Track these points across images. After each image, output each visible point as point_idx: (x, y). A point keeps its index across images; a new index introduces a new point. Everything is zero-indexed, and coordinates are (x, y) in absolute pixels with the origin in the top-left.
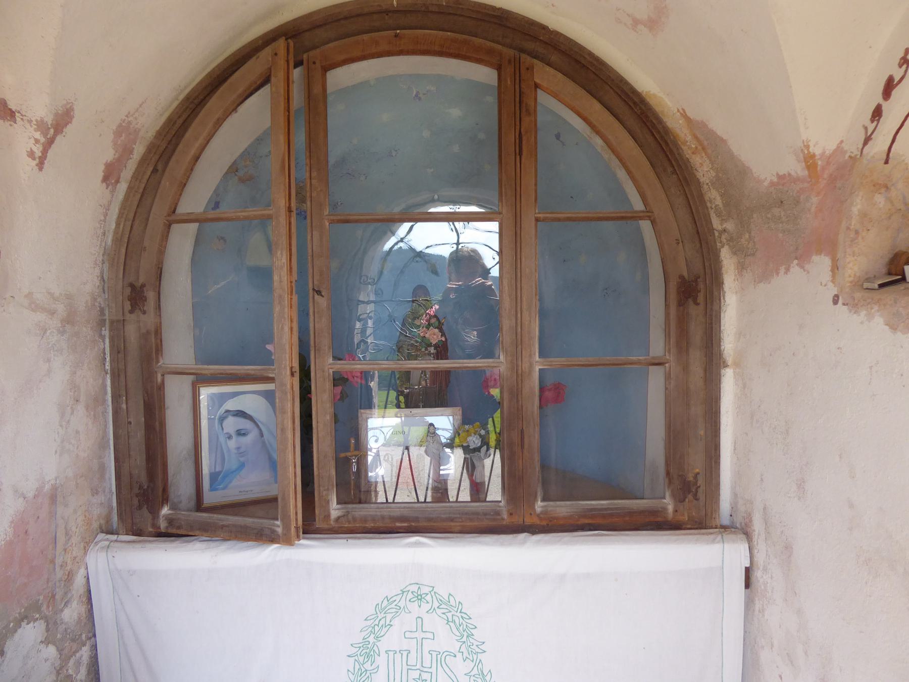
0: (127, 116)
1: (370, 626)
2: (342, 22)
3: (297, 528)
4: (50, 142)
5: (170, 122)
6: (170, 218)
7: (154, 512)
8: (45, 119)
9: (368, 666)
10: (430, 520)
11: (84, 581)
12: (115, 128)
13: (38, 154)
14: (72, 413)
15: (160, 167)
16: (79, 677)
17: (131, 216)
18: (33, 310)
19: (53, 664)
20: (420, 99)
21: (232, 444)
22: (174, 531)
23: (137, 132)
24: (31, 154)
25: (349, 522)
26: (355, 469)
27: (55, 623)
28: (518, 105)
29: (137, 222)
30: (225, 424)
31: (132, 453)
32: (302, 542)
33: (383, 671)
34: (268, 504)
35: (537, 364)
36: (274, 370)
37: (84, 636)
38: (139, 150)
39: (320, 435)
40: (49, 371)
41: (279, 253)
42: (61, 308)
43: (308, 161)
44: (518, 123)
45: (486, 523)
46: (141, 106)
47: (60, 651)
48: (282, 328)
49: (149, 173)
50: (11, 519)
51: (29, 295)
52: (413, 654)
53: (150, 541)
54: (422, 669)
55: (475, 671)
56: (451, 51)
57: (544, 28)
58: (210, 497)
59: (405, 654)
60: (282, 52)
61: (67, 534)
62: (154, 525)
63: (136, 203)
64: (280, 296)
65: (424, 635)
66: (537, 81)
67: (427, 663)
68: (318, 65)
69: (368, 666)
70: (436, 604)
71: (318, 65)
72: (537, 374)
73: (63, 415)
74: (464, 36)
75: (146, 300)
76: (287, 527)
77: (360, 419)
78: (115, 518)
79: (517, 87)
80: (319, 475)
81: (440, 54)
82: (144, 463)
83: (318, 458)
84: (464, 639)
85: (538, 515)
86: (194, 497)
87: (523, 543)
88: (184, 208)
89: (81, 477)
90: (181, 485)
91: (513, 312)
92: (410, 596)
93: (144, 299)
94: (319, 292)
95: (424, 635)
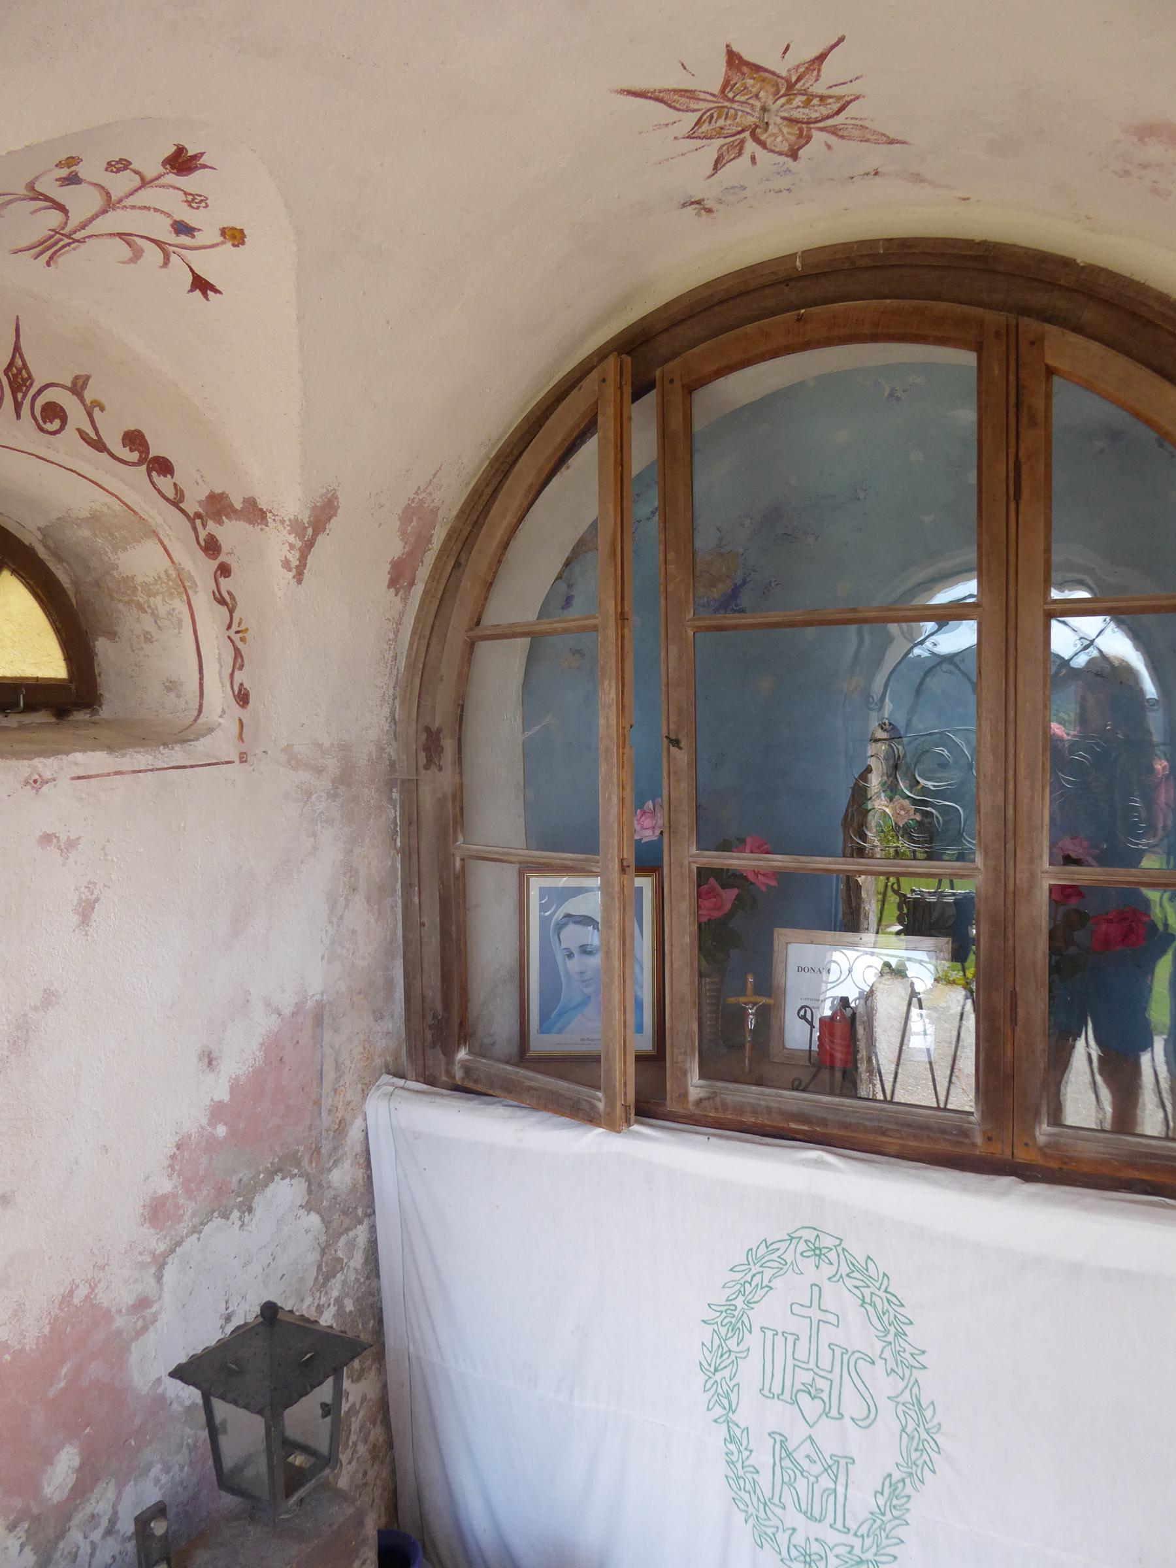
0: (416, 493)
1: (737, 1282)
2: (717, 309)
3: (626, 1107)
4: (310, 545)
5: (476, 494)
6: (471, 634)
7: (449, 1055)
8: (300, 517)
9: (732, 1343)
10: (846, 1126)
11: (361, 1136)
12: (400, 512)
13: (295, 562)
14: (347, 906)
15: (462, 561)
16: (352, 1264)
17: (427, 633)
18: (293, 768)
19: (316, 1238)
20: (898, 399)
21: (574, 965)
22: (470, 1085)
23: (434, 512)
24: (286, 564)
25: (716, 1109)
26: (751, 1024)
27: (320, 1185)
28: (1012, 410)
29: (435, 639)
30: (579, 933)
31: (425, 967)
32: (636, 1127)
33: (755, 1358)
34: (581, 1066)
35: (1048, 875)
36: (598, 862)
37: (360, 1211)
38: (439, 536)
39: (675, 966)
40: (315, 848)
41: (607, 683)
42: (332, 765)
43: (662, 536)
44: (1013, 442)
45: (943, 1147)
46: (434, 476)
47: (326, 1222)
48: (610, 798)
49: (449, 569)
50: (261, 1040)
51: (288, 749)
52: (803, 1344)
53: (442, 1095)
54: (816, 1370)
55: (906, 1397)
56: (892, 331)
57: (1067, 263)
58: (540, 1043)
59: (791, 1339)
60: (612, 377)
61: (337, 1069)
62: (449, 1073)
63: (433, 613)
64: (607, 750)
65: (822, 1316)
66: (1050, 361)
67: (825, 1363)
68: (677, 383)
69: (732, 1343)
70: (844, 1269)
71: (677, 383)
72: (1047, 893)
73: (333, 908)
74: (915, 302)
75: (442, 751)
76: (611, 1103)
77: (776, 943)
78: (404, 1058)
79: (1012, 378)
80: (672, 1028)
81: (874, 338)
82: (439, 984)
83: (672, 1002)
84: (890, 1338)
85: (1041, 1149)
86: (517, 1038)
87: (1004, 1193)
88: (499, 613)
89: (359, 993)
90: (496, 1018)
91: (1000, 780)
92: (802, 1246)
93: (440, 750)
94: (676, 743)
95: (822, 1316)
